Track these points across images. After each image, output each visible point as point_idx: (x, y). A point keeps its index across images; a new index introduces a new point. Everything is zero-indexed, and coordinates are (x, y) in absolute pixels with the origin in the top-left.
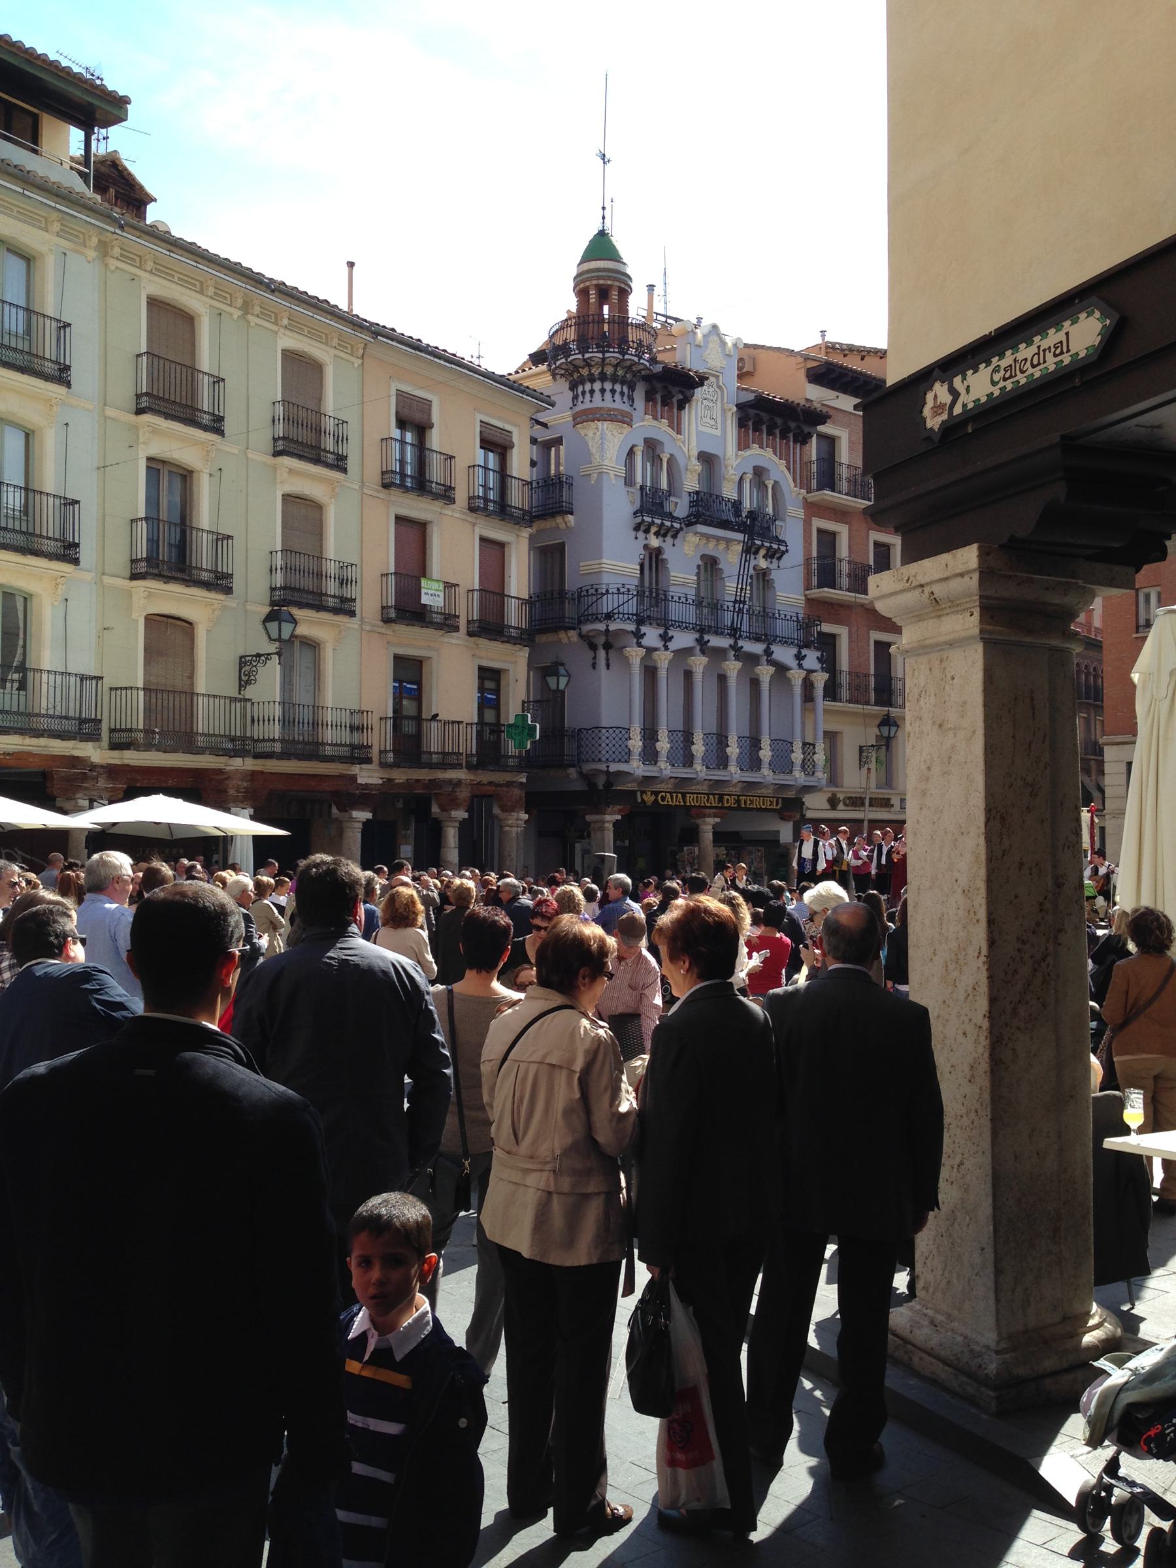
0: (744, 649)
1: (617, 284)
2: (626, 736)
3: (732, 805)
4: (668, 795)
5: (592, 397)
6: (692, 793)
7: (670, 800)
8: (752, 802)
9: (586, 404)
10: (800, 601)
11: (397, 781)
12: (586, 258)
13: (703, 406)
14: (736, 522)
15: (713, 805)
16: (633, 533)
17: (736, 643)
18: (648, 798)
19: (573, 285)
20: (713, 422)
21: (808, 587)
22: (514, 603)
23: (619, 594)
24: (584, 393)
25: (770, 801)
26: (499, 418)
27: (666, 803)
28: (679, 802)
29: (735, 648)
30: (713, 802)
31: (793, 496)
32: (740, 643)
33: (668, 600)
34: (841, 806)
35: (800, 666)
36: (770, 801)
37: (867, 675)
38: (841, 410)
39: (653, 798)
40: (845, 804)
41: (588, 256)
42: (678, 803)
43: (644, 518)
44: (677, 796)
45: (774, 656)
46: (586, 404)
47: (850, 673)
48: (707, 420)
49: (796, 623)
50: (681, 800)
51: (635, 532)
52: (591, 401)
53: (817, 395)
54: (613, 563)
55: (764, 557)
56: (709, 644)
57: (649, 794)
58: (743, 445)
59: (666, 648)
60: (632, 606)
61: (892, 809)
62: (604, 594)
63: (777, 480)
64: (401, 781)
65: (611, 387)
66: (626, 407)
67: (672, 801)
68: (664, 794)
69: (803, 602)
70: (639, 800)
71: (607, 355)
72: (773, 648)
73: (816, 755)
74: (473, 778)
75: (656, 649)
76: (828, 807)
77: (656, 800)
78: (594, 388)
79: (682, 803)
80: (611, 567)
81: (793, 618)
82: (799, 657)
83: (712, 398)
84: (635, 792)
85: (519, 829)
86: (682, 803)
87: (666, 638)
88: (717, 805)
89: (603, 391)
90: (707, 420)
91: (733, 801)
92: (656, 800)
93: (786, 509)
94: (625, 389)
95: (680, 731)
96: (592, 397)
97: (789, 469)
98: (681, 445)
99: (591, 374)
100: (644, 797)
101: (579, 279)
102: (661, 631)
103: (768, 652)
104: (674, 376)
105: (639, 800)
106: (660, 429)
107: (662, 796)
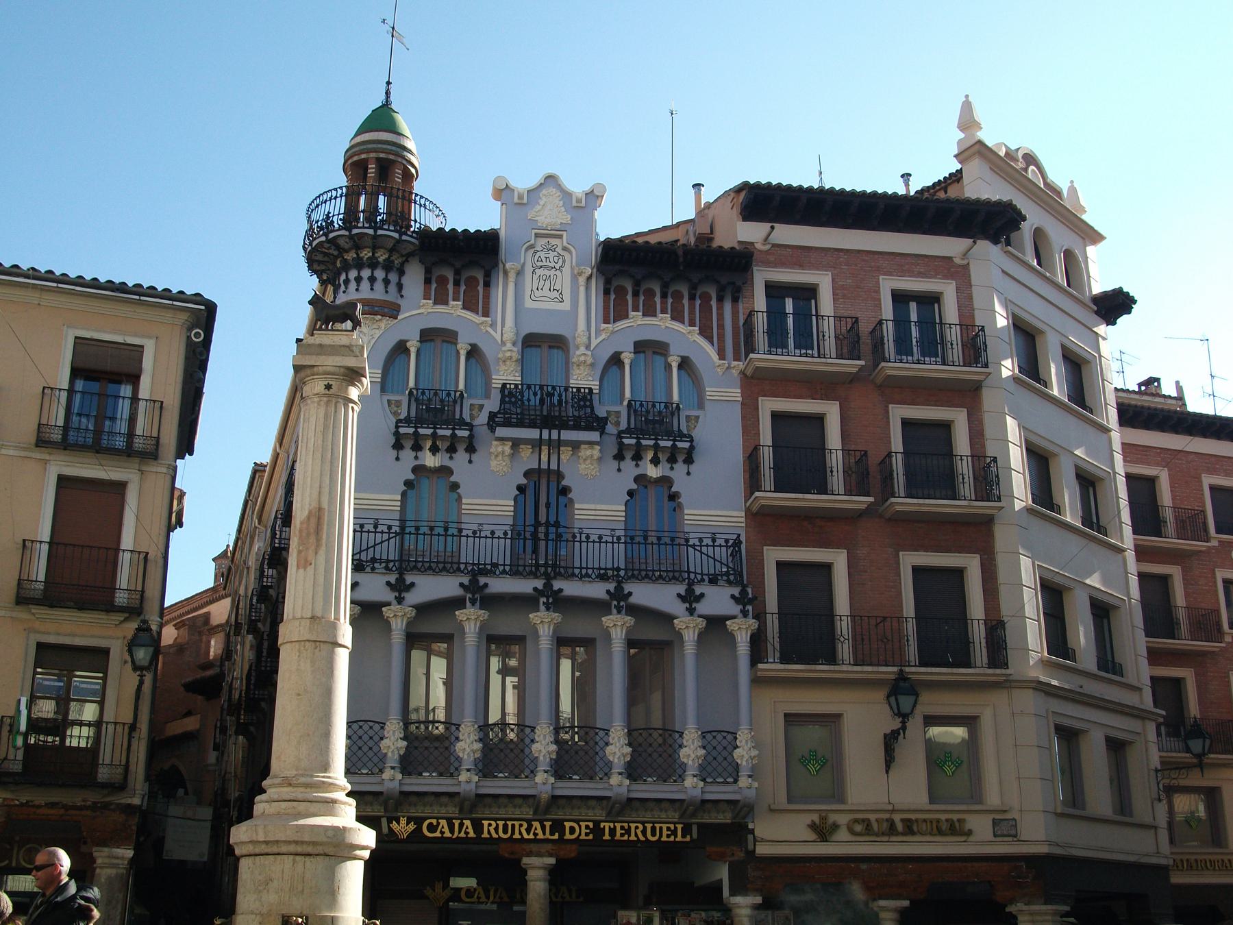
1: (372, 155)
3: (583, 837)
4: (443, 822)
6: (495, 820)
7: (446, 829)
13: (535, 277)
14: (574, 416)
15: (541, 836)
17: (548, 585)
20: (555, 294)
22: (127, 556)
23: (474, 537)
25: (668, 829)
26: (114, 332)
27: (438, 834)
28: (466, 833)
29: (547, 591)
32: (557, 585)
34: (843, 834)
35: (691, 611)
36: (668, 829)
37: (900, 619)
38: (817, 248)
39: (412, 827)
40: (851, 831)
41: (365, 127)
42: (462, 835)
44: (461, 825)
45: (632, 600)
47: (853, 616)
49: (724, 549)
51: (395, 452)
53: (752, 233)
54: (377, 496)
55: (652, 461)
57: (403, 821)
58: (614, 312)
59: (400, 600)
61: (971, 838)
63: (686, 355)
65: (370, 274)
66: (392, 296)
67: (452, 831)
71: (380, 232)
72: (628, 588)
73: (737, 751)
75: (389, 604)
76: (813, 836)
77: (418, 830)
78: (389, 277)
80: (598, 513)
81: (637, 539)
82: (690, 599)
83: (552, 264)
87: (400, 588)
88: (548, 836)
90: (546, 292)
91: (584, 831)
92: (418, 830)
93: (705, 391)
94: (380, 274)
97: (710, 339)
98: (489, 329)
99: (359, 258)
100: (394, 825)
103: (619, 595)
106: (453, 314)
107: (431, 824)
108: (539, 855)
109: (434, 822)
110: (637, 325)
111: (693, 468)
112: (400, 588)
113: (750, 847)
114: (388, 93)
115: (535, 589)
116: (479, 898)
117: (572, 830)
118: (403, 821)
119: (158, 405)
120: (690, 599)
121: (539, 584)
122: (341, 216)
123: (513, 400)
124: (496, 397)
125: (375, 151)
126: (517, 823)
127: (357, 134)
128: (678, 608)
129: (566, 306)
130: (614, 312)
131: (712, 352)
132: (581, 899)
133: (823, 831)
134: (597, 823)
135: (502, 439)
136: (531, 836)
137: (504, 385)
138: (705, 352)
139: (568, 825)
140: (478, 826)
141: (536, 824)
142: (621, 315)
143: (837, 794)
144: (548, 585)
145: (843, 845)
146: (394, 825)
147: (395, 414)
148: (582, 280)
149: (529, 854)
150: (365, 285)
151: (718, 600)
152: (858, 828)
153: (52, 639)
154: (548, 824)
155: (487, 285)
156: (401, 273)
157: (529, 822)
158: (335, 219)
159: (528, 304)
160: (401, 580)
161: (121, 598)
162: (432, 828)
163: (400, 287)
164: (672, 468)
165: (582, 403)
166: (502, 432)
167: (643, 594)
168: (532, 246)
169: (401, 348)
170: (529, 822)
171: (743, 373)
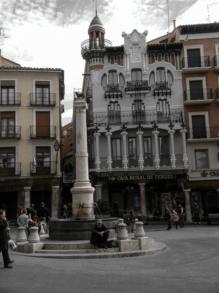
0: (158, 127)
1: (94, 30)
2: (107, 160)
4: (121, 177)
5: (94, 62)
6: (132, 176)
7: (122, 178)
8: (161, 177)
9: (92, 64)
10: (182, 107)
11: (1, 180)
12: (91, 25)
15: (142, 179)
16: (105, 99)
17: (140, 126)
18: (113, 179)
19: (88, 32)
20: (138, 59)
21: (185, 98)
24: (91, 61)
28: (126, 179)
29: (140, 127)
30: (142, 178)
31: (178, 77)
33: (162, 115)
34: (209, 175)
35: (171, 129)
36: (169, 176)
39: (115, 178)
42: (126, 179)
43: (118, 93)
44: (125, 177)
46: (92, 64)
48: (136, 58)
50: (127, 178)
51: (154, 96)
52: (94, 63)
56: (126, 128)
57: (113, 177)
60: (106, 121)
62: (96, 118)
64: (3, 180)
66: (101, 64)
67: (123, 179)
68: (120, 177)
69: (183, 107)
70: (110, 180)
74: (34, 177)
76: (201, 176)
78: (94, 59)
79: (128, 179)
82: (171, 126)
84: (108, 177)
85: (56, 191)
86: (128, 179)
88: (144, 179)
89: (97, 60)
90: (136, 58)
92: (116, 179)
95: (115, 157)
96: (94, 62)
97: (174, 65)
99: (93, 56)
100: (111, 178)
101: (89, 30)
102: (169, 124)
103: (155, 127)
104: (179, 46)
105: (110, 180)
106: (116, 66)
108: (142, 183)
109: (120, 177)
110: (158, 64)
111: (171, 96)
112: (108, 129)
113: (188, 179)
114: (96, 13)
115: (137, 127)
116: (132, 191)
117: (149, 177)
118: (113, 177)
119: (20, 94)
120: (171, 126)
121: (138, 126)
122: (88, 47)
123: (130, 85)
124: (126, 84)
125: (95, 29)
126: (137, 176)
127: (90, 25)
128: (168, 129)
129: (140, 61)
130: (152, 61)
131: (175, 68)
132: (154, 191)
133: (204, 175)
134: (154, 176)
135: (128, 94)
136: (140, 179)
137: (128, 82)
138: (173, 69)
139: (148, 176)
140: (129, 177)
141: (141, 176)
142: (153, 62)
143: (208, 166)
144: (140, 126)
145: (209, 178)
146: (111, 178)
147: (105, 90)
148: (144, 55)
149: (140, 183)
150: (95, 62)
151: (177, 126)
152: (212, 174)
153: (39, 145)
154: (143, 176)
155: (122, 58)
156: (103, 58)
157: (139, 176)
158: (87, 47)
159: (132, 62)
160: (171, 124)
161: (52, 136)
162: (119, 178)
163: (103, 61)
164: (166, 97)
165: (145, 84)
166: (128, 92)
167: (161, 126)
168: (132, 48)
169: (105, 75)
170: (139, 176)
171: (182, 72)
